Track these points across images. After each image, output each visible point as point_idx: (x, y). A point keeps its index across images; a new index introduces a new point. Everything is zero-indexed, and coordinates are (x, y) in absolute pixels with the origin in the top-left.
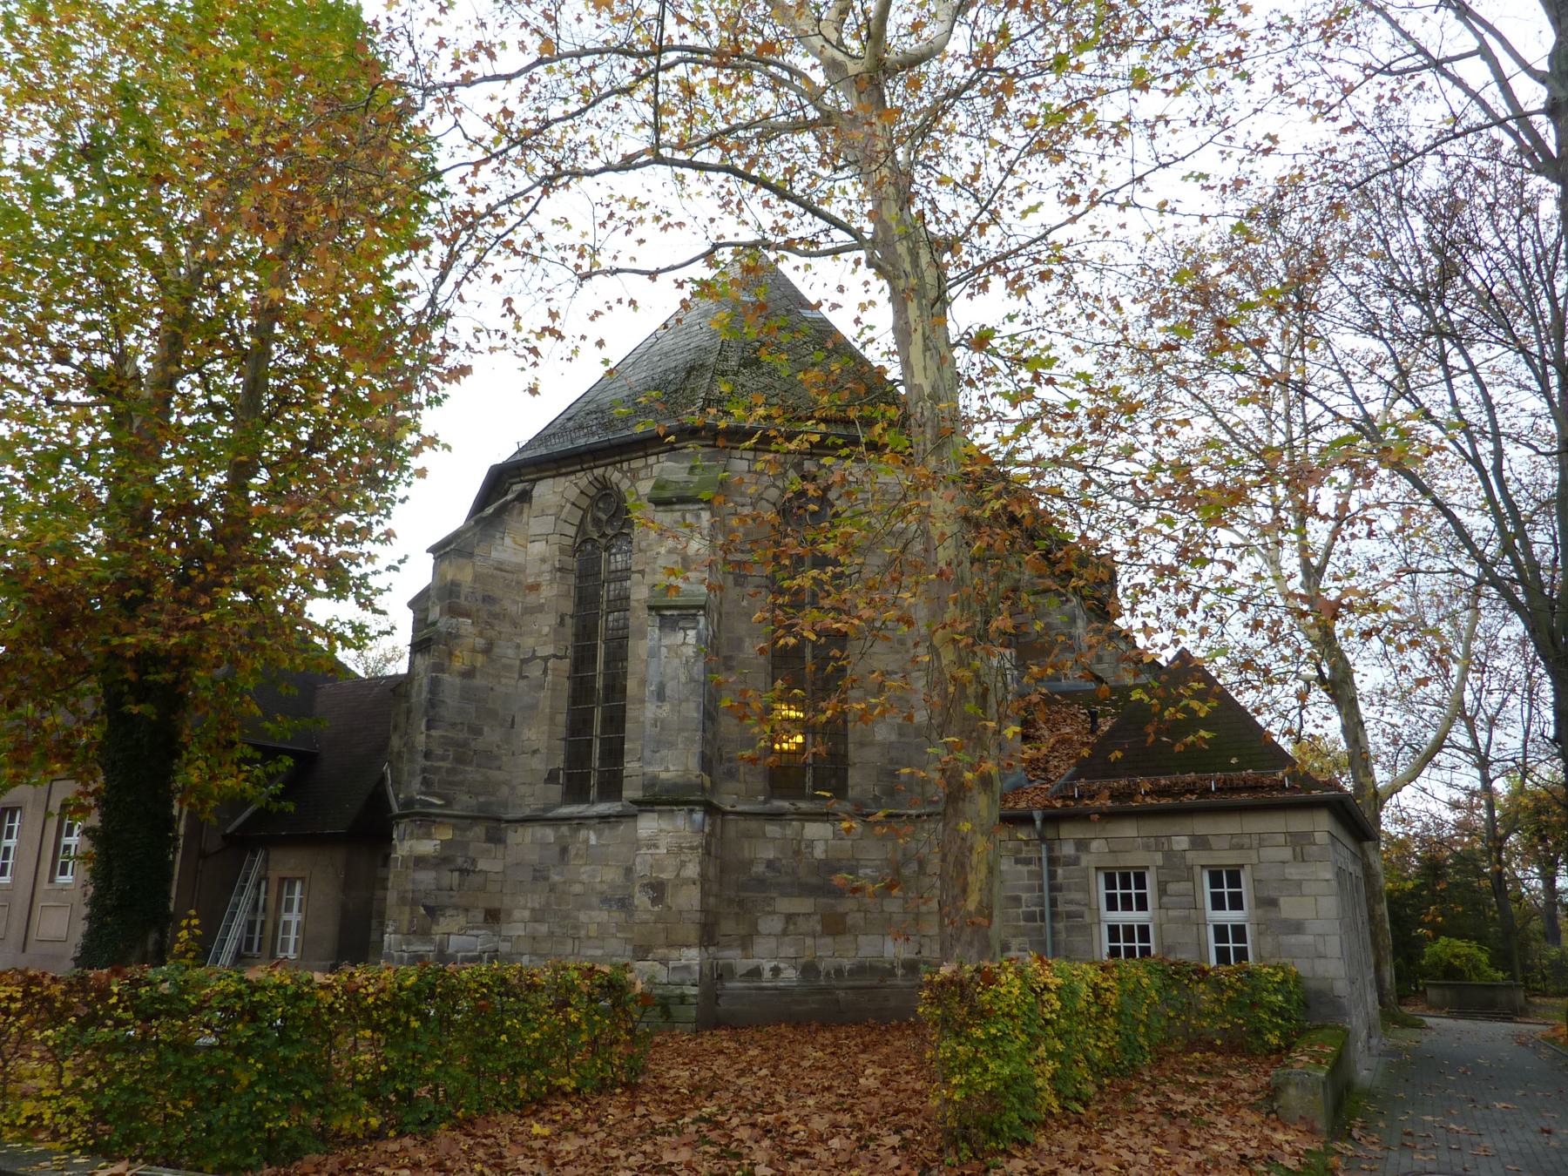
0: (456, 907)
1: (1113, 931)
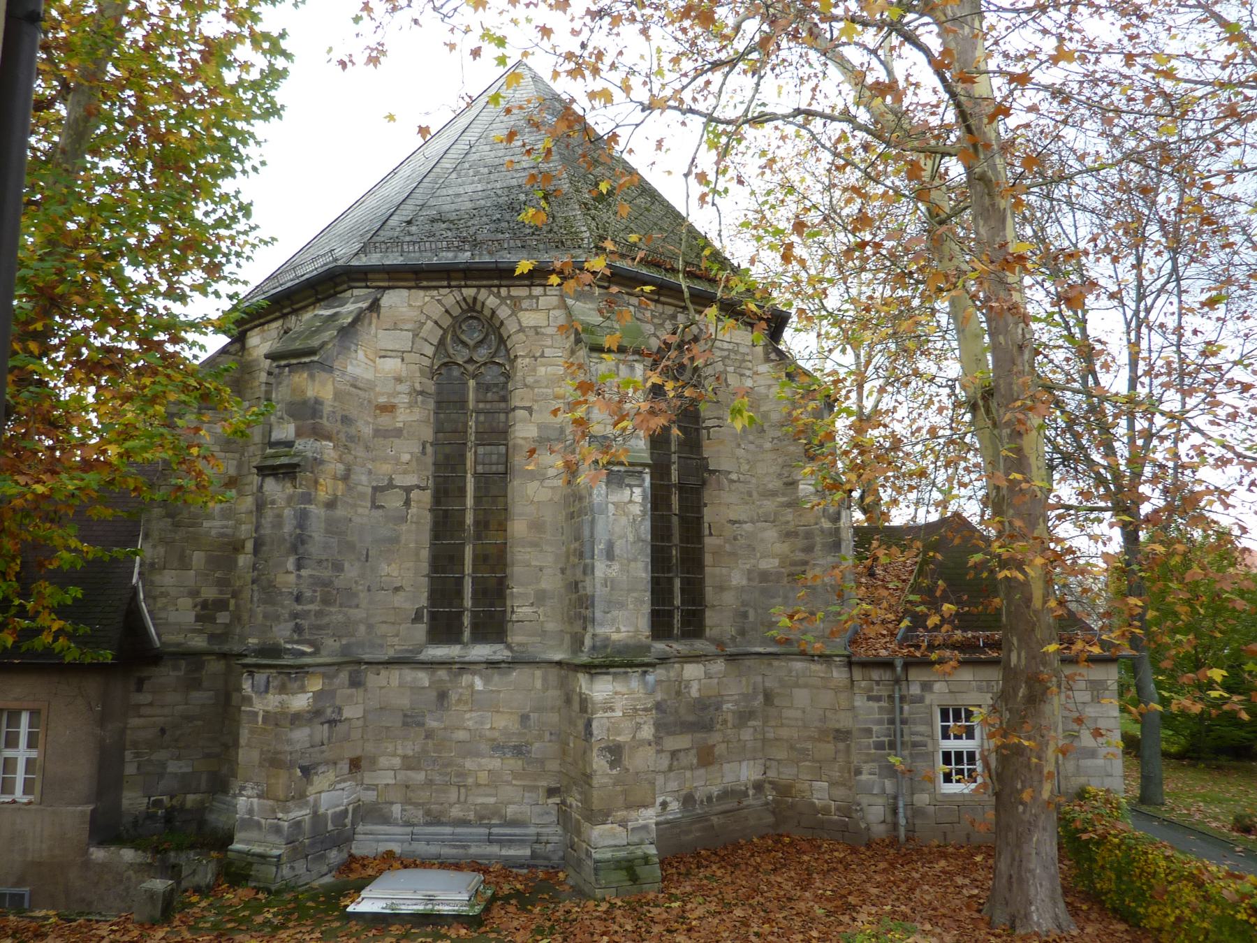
0: (326, 763)
1: (947, 757)
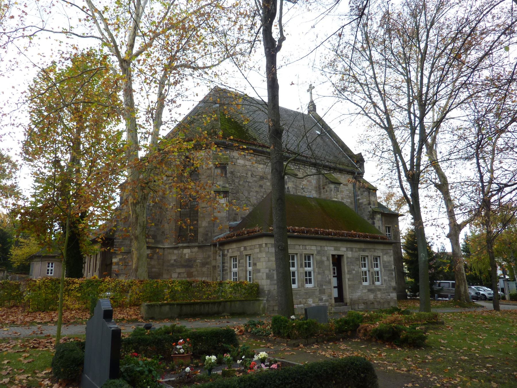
0: (123, 274)
